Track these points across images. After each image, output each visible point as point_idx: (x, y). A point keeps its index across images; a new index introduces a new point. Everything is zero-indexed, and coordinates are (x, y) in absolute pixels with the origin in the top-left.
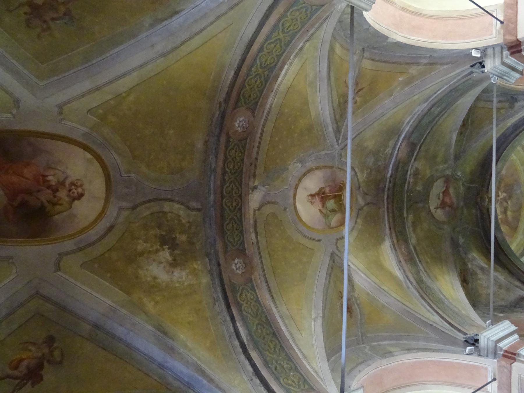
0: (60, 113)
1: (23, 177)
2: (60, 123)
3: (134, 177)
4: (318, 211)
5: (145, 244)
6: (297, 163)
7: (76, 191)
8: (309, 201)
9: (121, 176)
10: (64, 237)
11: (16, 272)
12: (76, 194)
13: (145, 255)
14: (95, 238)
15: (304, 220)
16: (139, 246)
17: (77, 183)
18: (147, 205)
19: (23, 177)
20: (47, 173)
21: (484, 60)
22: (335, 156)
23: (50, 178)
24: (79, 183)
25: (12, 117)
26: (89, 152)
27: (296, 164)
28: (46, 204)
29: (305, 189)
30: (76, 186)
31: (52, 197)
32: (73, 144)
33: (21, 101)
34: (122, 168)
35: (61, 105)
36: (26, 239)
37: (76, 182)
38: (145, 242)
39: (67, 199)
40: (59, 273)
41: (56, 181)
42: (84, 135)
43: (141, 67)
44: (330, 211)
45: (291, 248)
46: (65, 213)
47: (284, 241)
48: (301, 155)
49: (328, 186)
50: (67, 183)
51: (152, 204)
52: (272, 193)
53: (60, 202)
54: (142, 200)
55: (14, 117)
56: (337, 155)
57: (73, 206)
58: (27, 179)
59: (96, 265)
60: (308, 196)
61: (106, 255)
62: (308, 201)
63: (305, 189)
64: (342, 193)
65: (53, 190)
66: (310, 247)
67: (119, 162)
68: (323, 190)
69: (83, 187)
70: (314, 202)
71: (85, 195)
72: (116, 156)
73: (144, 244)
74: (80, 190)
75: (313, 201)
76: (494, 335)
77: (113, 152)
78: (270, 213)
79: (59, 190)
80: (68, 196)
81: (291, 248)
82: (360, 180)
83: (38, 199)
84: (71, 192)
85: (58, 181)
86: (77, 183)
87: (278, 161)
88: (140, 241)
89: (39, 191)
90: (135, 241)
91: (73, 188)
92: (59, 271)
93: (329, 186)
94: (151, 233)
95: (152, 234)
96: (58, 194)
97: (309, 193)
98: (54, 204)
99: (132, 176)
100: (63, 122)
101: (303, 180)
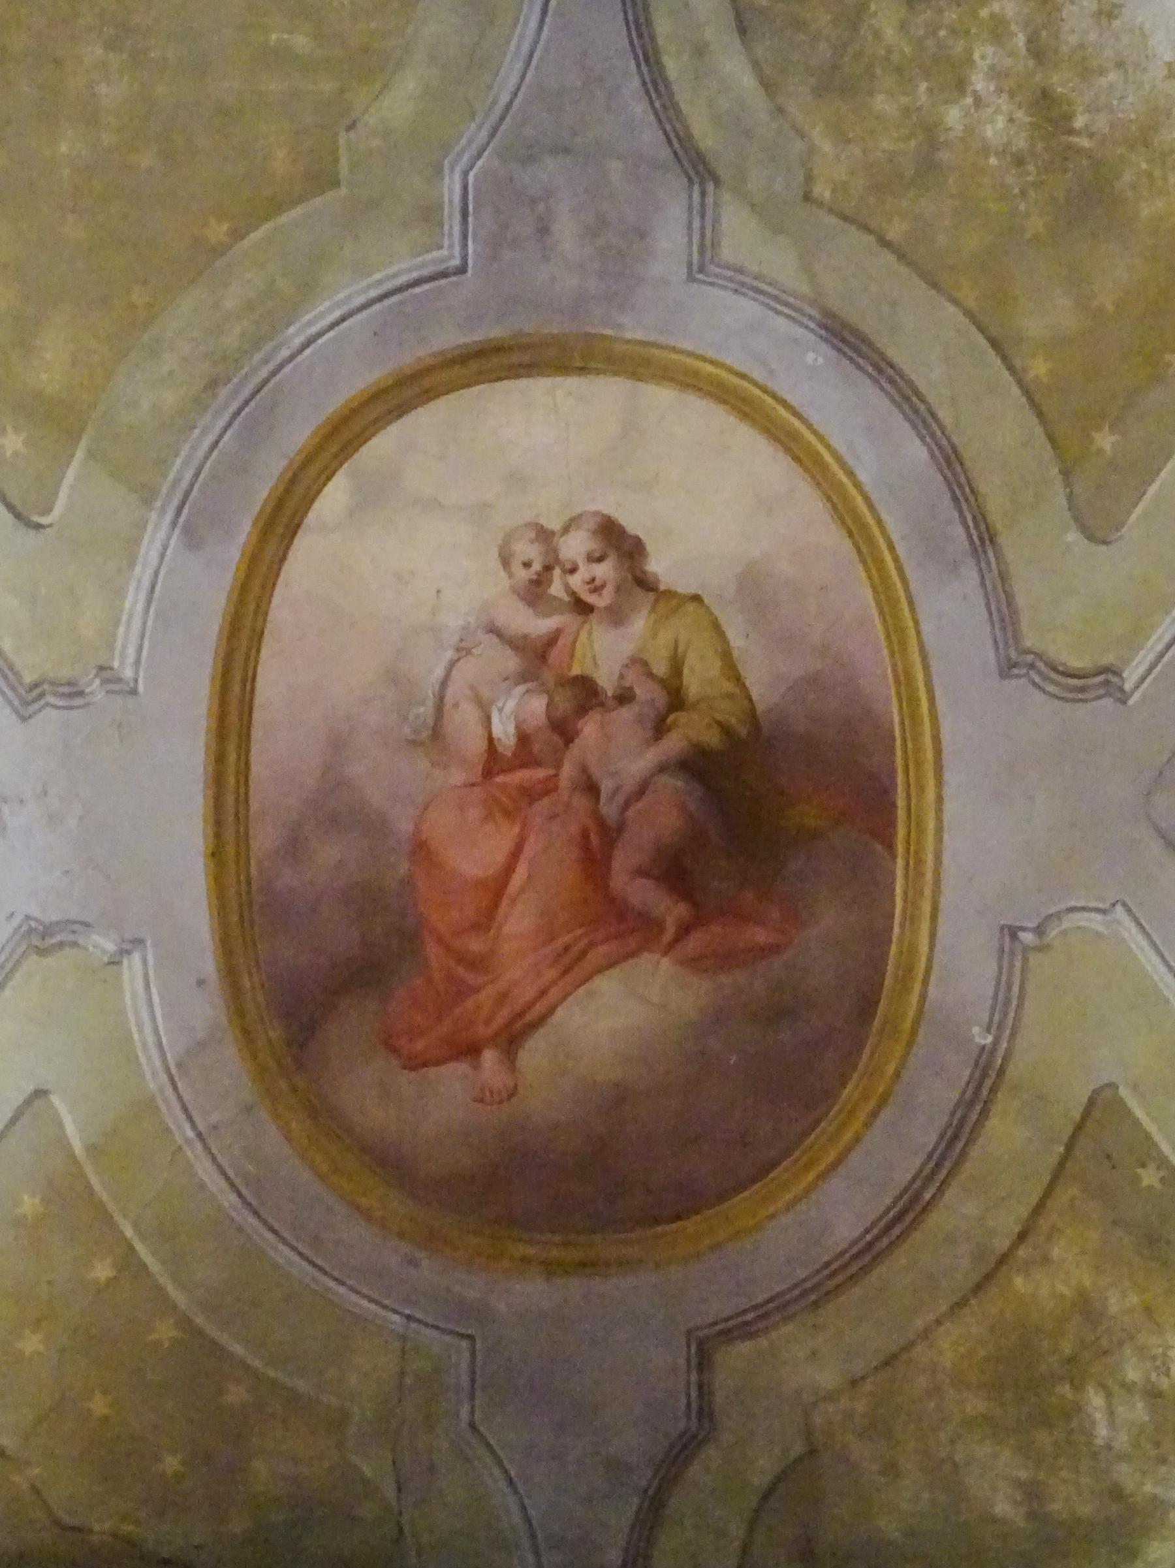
0: (74, 692)
1: (509, 869)
2: (134, 692)
3: (465, 174)
5: (979, 83)
7: (584, 573)
9: (462, 270)
10: (896, 634)
11: (1103, 912)
12: (605, 571)
13: (1060, 82)
14: (917, 452)
16: (989, 133)
17: (527, 565)
18: (672, 66)
19: (509, 869)
20: (475, 746)
21: (653, 616)
23: (504, 730)
24: (527, 549)
25: (136, 957)
26: (309, 500)
28: (673, 744)
30: (548, 568)
31: (626, 714)
32: (262, 611)
33: (28, 918)
34: (404, 268)
35: (20, 697)
36: (890, 847)
37: (523, 575)
38: (961, 86)
39: (640, 623)
40: (1131, 677)
41: (521, 689)
42: (193, 538)
46: (736, 641)
50: (540, 626)
51: (663, 27)
53: (661, 668)
54: (639, 109)
55: (139, 942)
57: (684, 585)
58: (515, 855)
59: (1105, 441)
61: (1039, 368)
65: (582, 710)
67: (357, 291)
69: (555, 525)
71: (608, 511)
72: (323, 311)
73: (975, 92)
74: (576, 546)
77: (295, 335)
79: (576, 671)
80: (616, 616)
83: (642, 789)
84: (591, 599)
85: (524, 677)
86: (527, 565)
88: (953, 116)
89: (591, 788)
90: (944, 156)
91: (567, 587)
92: (1118, 674)
94: (890, 33)
95: (903, 26)
96: (606, 680)
98: (676, 700)
99: (458, 188)
100: (128, 673)
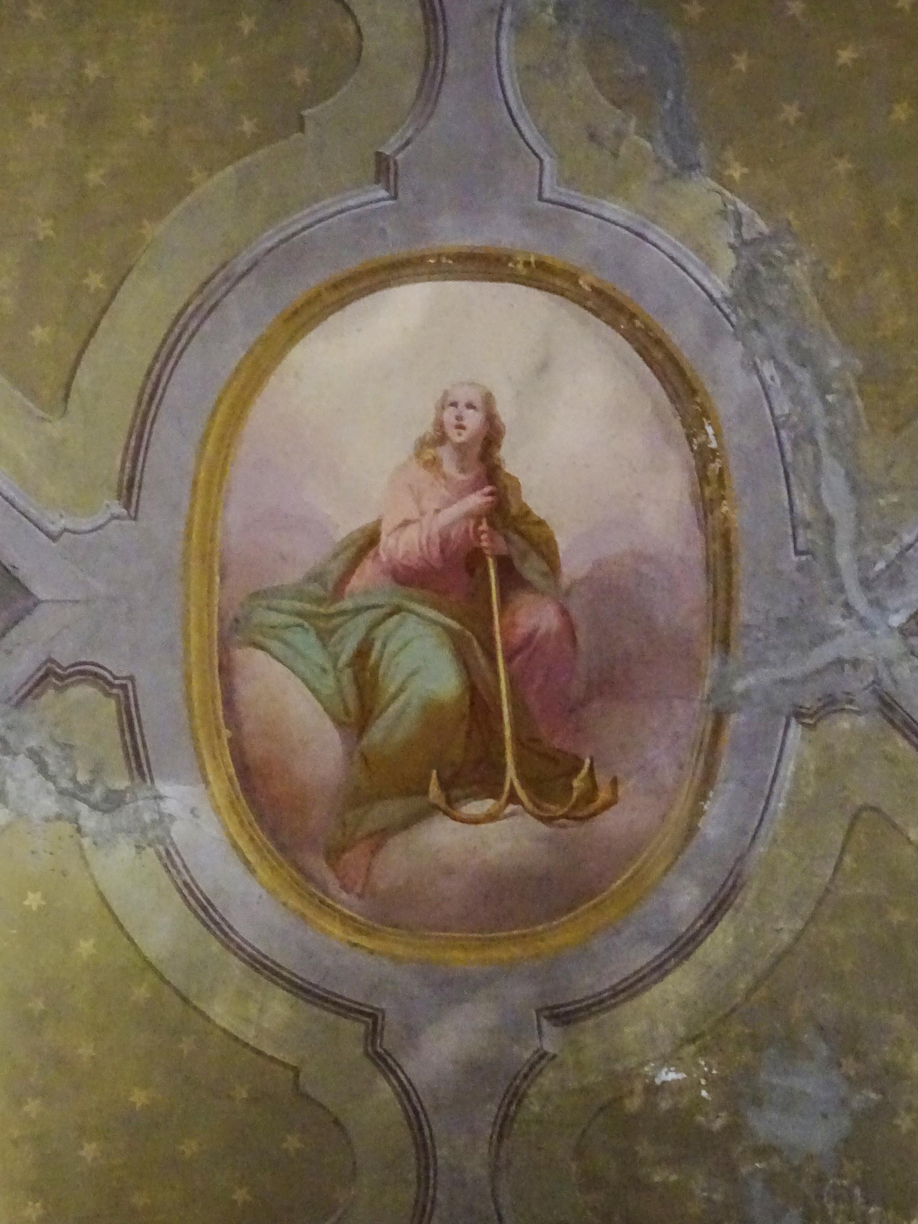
4: (366, 520)
6: (740, 246)
8: (449, 416)
15: (298, 354)
22: (823, 636)
27: (728, 234)
29: (543, 367)
43: (512, 1090)
44: (362, 653)
45: (94, 177)
47: (145, 124)
48: (798, 271)
49: (570, 628)
52: (504, 44)
56: (826, 653)
60: (488, 399)
62: (447, 403)
63: (543, 367)
64: (513, 798)
66: (84, 380)
68: (532, 569)
70: (434, 464)
75: (445, 454)
76: (31, 520)
78: (359, 30)
81: (94, 177)
82: (627, 1009)
87: (742, 63)
93: (570, 628)
97: (505, 412)
101: (607, 331)
